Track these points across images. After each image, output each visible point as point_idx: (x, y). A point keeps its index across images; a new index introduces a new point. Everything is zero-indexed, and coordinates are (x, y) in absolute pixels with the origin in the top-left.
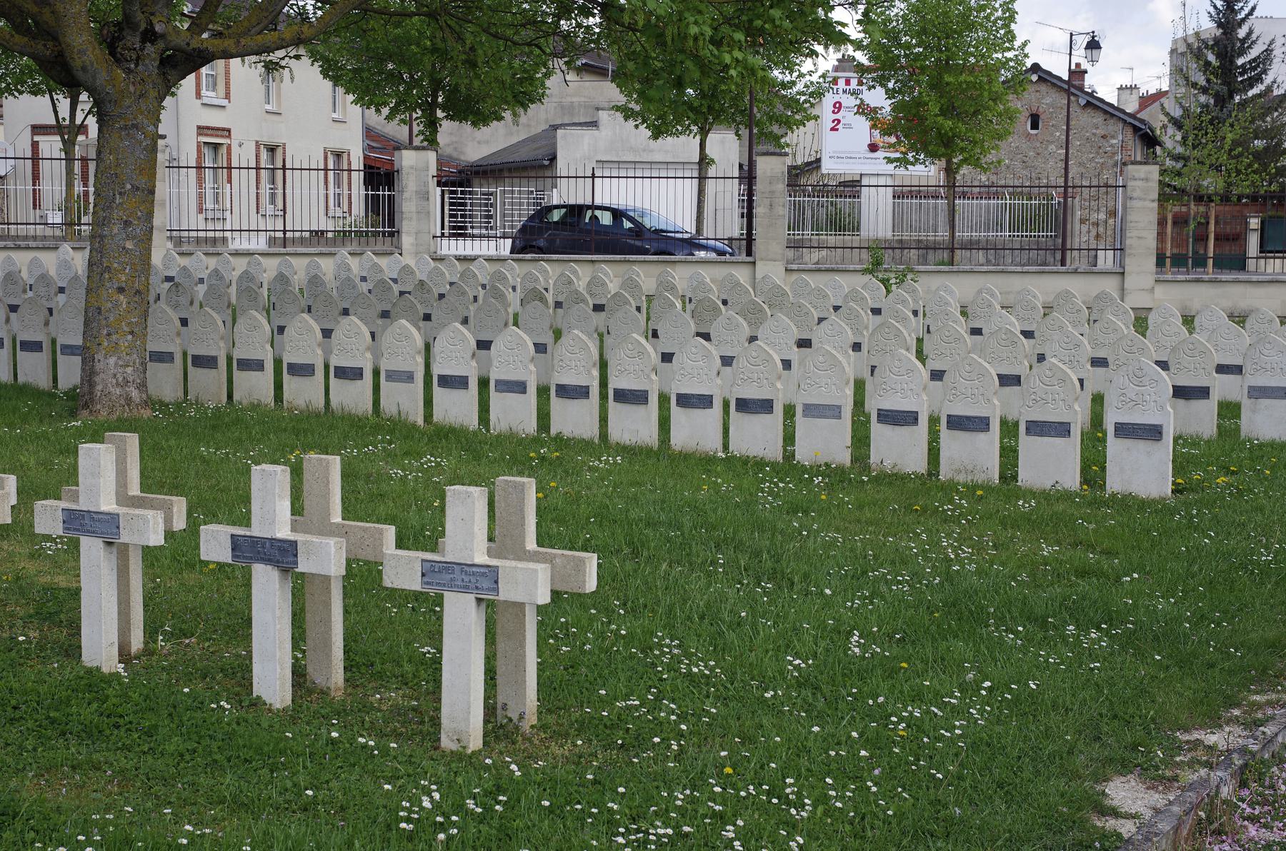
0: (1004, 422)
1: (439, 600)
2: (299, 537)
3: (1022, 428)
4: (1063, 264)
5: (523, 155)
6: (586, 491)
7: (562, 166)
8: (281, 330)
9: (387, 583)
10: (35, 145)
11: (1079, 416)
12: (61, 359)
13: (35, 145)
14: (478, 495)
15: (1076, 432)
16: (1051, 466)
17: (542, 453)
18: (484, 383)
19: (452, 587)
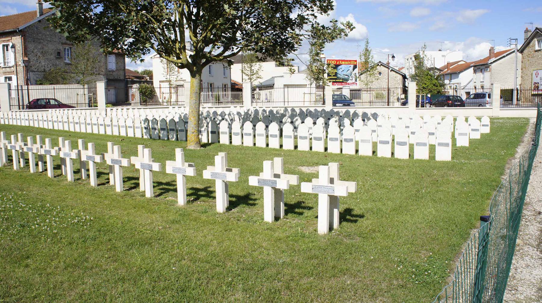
0: (410, 144)
1: (263, 188)
2: (151, 163)
3: (415, 145)
4: (388, 105)
5: (268, 83)
6: (350, 167)
7: (275, 86)
8: (342, 130)
9: (167, 172)
10: (160, 85)
11: (390, 139)
12: (121, 129)
13: (160, 85)
14: (269, 162)
15: (390, 143)
16: (422, 154)
17: (340, 157)
18: (105, 125)
19: (321, 192)
